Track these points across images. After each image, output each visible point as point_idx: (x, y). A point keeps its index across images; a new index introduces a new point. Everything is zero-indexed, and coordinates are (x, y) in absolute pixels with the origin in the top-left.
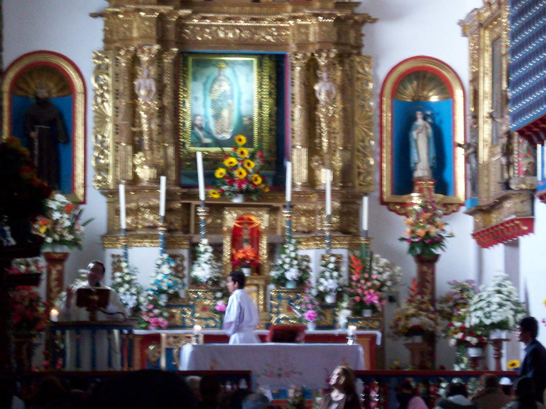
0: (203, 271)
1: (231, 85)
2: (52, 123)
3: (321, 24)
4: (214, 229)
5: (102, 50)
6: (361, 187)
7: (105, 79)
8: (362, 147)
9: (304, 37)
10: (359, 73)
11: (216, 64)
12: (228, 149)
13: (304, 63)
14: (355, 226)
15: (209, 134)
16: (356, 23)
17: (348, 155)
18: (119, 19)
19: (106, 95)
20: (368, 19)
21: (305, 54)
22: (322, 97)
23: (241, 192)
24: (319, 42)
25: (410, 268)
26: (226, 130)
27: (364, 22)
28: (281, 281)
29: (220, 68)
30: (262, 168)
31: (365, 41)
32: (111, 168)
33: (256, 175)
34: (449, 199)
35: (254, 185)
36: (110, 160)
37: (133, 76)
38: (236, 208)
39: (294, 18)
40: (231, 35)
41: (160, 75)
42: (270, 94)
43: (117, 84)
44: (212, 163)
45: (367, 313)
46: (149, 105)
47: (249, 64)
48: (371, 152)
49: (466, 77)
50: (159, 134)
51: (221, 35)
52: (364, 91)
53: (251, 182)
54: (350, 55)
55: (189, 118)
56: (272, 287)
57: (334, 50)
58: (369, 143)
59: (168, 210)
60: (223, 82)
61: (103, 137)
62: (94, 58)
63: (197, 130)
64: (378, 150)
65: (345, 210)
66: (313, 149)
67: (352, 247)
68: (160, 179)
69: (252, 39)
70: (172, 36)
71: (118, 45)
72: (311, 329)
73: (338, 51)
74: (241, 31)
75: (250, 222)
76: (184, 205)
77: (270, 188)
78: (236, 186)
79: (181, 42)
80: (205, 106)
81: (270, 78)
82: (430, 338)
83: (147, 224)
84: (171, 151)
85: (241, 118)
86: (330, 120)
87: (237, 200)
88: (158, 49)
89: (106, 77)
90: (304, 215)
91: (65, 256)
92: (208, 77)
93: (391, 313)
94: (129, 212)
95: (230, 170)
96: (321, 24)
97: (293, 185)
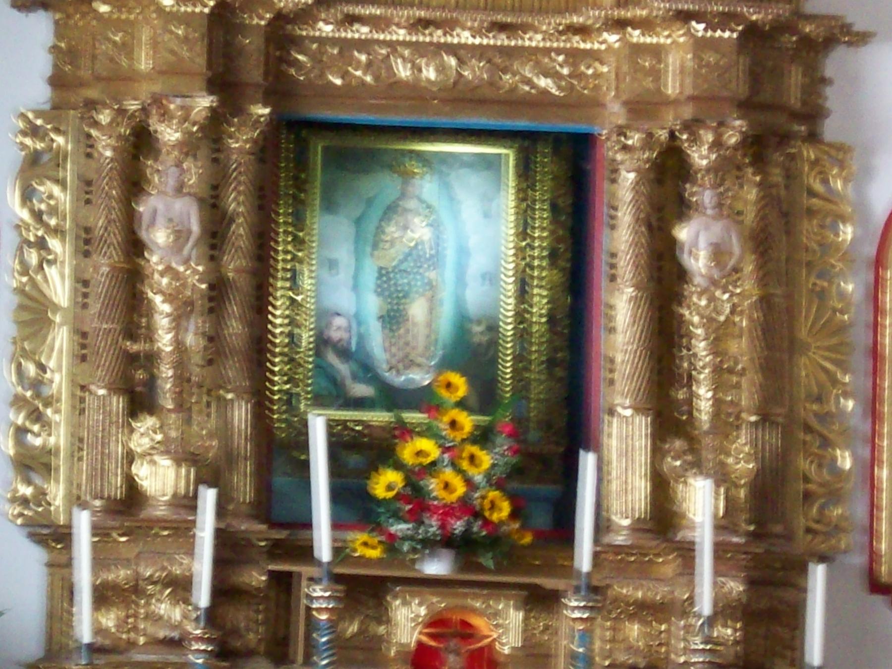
1: (435, 226)
3: (700, 45)
5: (47, 107)
6: (810, 537)
7: (51, 197)
8: (816, 415)
9: (648, 83)
10: (812, 193)
11: (394, 164)
12: (413, 417)
13: (648, 160)
14: (788, 653)
15: (367, 370)
16: (807, 42)
17: (773, 439)
18: (99, 17)
19: (54, 243)
20: (841, 34)
21: (650, 135)
22: (698, 263)
23: (448, 541)
24: (692, 98)
26: (420, 360)
27: (829, 42)
29: (407, 176)
30: (517, 472)
31: (832, 98)
32: (62, 463)
33: (494, 494)
35: (487, 523)
36: (59, 438)
37: (134, 185)
38: (426, 590)
39: (620, 25)
40: (430, 73)
41: (215, 187)
42: (553, 256)
43: (84, 211)
44: (359, 454)
46: (176, 276)
47: (490, 164)
48: (844, 432)
50: (210, 362)
51: (403, 72)
52: (827, 247)
53: (477, 514)
54: (785, 138)
55: (311, 323)
57: (738, 123)
58: (838, 402)
59: (223, 591)
60: (410, 217)
61: (42, 368)
62: (24, 133)
63: (332, 358)
64: (866, 427)
65: (764, 604)
66: (668, 419)
68: (195, 496)
69: (491, 84)
70: (253, 71)
71: (92, 93)
73: (750, 126)
74: (461, 62)
75: (466, 632)
76: (275, 576)
77: (539, 535)
78: (433, 525)
79: (279, 89)
80: (356, 288)
81: (554, 208)
83: (162, 634)
84: (241, 414)
85: (462, 322)
86: (719, 335)
87: (436, 567)
88: (211, 109)
89: (56, 190)
90: (632, 617)
92: (370, 202)
94: (103, 596)
95: (414, 479)
96: (700, 45)
97: (602, 526)
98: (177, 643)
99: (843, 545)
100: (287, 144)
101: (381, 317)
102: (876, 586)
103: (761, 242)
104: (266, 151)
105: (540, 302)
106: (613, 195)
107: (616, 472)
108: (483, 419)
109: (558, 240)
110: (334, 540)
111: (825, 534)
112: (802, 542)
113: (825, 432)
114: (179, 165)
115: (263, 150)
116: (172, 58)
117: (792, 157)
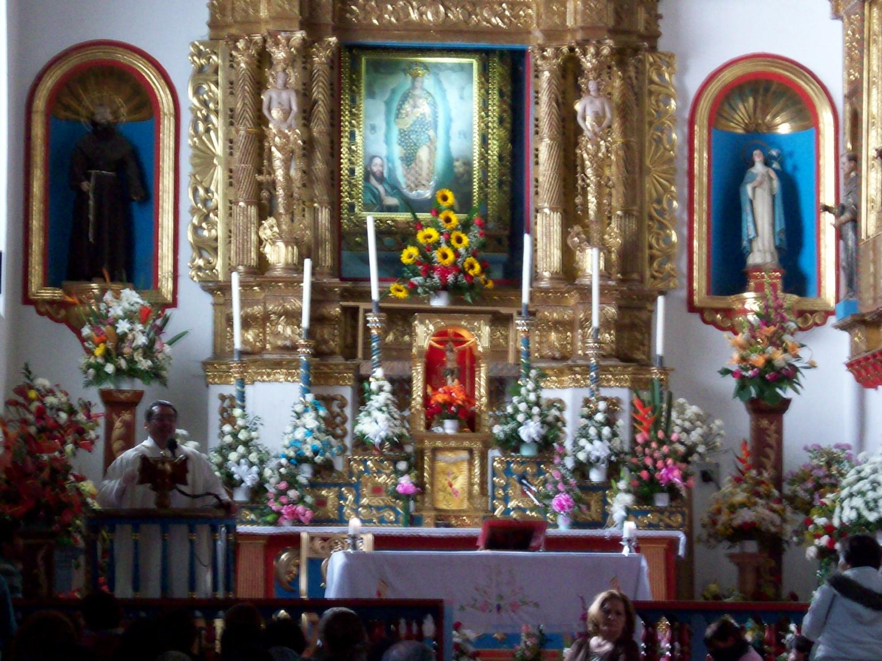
0: (375, 424)
1: (434, 105)
2: (120, 166)
4: (398, 352)
5: (207, 38)
10: (652, 82)
11: (408, 69)
12: (423, 216)
15: (395, 189)
21: (558, 49)
22: (588, 124)
23: (445, 287)
24: (582, 28)
25: (740, 422)
26: (424, 182)
28: (512, 443)
29: (415, 77)
30: (483, 247)
31: (663, 26)
33: (471, 259)
34: (808, 303)
36: (220, 231)
37: (259, 85)
42: (501, 121)
44: (393, 238)
45: (662, 500)
47: (465, 69)
49: (838, 90)
50: (304, 185)
54: (636, 50)
56: (495, 453)
57: (608, 41)
59: (317, 319)
63: (373, 181)
64: (685, 217)
65: (627, 321)
66: (571, 214)
67: (636, 386)
71: (234, 31)
72: (563, 528)
73: (616, 44)
75: (459, 340)
76: (345, 309)
79: (342, 27)
80: (387, 141)
81: (501, 94)
82: (773, 544)
83: (280, 343)
84: (324, 216)
85: (450, 162)
86: (600, 166)
91: (138, 396)
92: (393, 91)
93: (704, 499)
94: (246, 324)
95: (426, 252)
97: (535, 277)
98: (293, 348)
99: (672, 285)
100: (346, 58)
101: (850, 366)
102: (692, 308)
103: (624, 111)
104: (335, 63)
105: (494, 147)
106: (536, 85)
107: (543, 244)
108: (463, 216)
109: (504, 111)
110: (380, 287)
111: (661, 278)
112: (649, 284)
113: (661, 219)
114: (284, 70)
115: (332, 61)
116: (279, 9)
117: (640, 61)
